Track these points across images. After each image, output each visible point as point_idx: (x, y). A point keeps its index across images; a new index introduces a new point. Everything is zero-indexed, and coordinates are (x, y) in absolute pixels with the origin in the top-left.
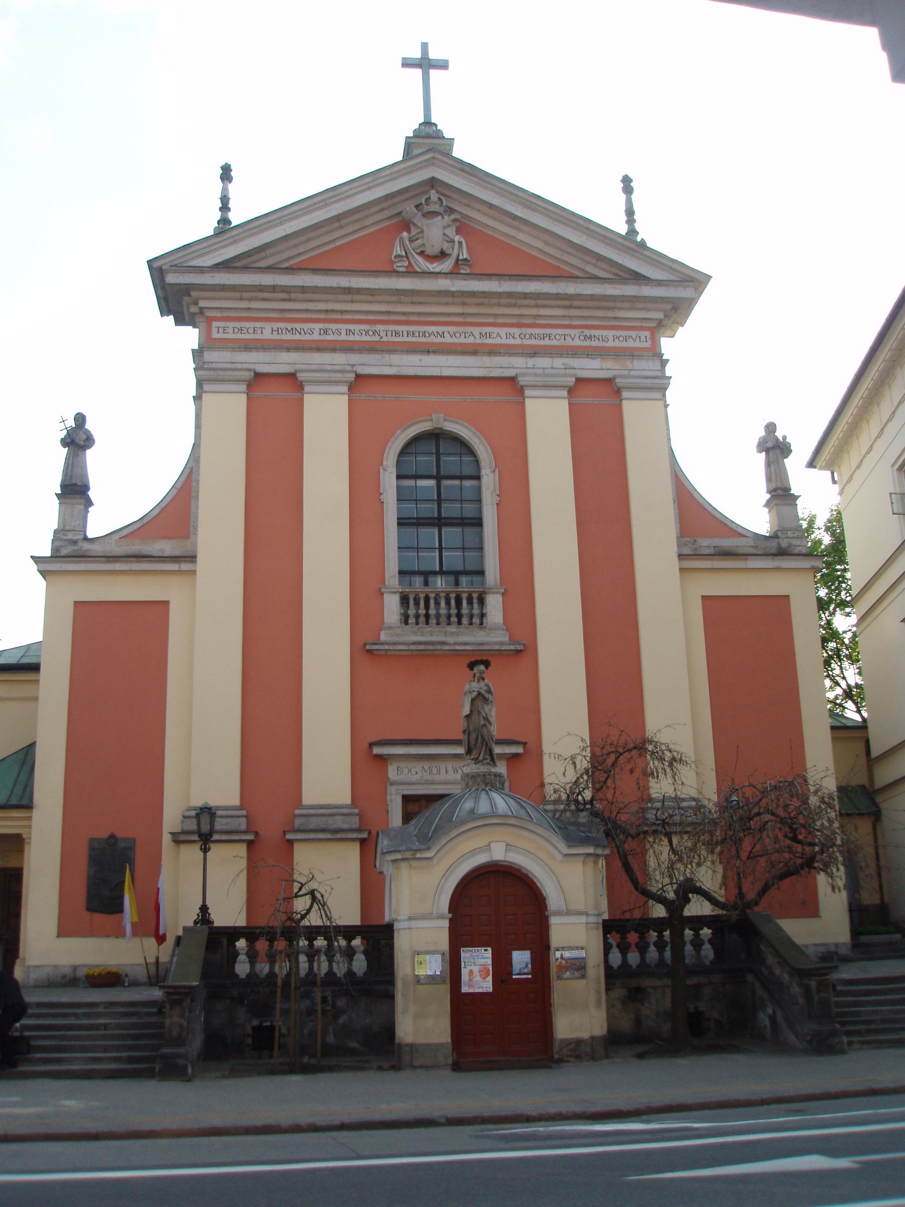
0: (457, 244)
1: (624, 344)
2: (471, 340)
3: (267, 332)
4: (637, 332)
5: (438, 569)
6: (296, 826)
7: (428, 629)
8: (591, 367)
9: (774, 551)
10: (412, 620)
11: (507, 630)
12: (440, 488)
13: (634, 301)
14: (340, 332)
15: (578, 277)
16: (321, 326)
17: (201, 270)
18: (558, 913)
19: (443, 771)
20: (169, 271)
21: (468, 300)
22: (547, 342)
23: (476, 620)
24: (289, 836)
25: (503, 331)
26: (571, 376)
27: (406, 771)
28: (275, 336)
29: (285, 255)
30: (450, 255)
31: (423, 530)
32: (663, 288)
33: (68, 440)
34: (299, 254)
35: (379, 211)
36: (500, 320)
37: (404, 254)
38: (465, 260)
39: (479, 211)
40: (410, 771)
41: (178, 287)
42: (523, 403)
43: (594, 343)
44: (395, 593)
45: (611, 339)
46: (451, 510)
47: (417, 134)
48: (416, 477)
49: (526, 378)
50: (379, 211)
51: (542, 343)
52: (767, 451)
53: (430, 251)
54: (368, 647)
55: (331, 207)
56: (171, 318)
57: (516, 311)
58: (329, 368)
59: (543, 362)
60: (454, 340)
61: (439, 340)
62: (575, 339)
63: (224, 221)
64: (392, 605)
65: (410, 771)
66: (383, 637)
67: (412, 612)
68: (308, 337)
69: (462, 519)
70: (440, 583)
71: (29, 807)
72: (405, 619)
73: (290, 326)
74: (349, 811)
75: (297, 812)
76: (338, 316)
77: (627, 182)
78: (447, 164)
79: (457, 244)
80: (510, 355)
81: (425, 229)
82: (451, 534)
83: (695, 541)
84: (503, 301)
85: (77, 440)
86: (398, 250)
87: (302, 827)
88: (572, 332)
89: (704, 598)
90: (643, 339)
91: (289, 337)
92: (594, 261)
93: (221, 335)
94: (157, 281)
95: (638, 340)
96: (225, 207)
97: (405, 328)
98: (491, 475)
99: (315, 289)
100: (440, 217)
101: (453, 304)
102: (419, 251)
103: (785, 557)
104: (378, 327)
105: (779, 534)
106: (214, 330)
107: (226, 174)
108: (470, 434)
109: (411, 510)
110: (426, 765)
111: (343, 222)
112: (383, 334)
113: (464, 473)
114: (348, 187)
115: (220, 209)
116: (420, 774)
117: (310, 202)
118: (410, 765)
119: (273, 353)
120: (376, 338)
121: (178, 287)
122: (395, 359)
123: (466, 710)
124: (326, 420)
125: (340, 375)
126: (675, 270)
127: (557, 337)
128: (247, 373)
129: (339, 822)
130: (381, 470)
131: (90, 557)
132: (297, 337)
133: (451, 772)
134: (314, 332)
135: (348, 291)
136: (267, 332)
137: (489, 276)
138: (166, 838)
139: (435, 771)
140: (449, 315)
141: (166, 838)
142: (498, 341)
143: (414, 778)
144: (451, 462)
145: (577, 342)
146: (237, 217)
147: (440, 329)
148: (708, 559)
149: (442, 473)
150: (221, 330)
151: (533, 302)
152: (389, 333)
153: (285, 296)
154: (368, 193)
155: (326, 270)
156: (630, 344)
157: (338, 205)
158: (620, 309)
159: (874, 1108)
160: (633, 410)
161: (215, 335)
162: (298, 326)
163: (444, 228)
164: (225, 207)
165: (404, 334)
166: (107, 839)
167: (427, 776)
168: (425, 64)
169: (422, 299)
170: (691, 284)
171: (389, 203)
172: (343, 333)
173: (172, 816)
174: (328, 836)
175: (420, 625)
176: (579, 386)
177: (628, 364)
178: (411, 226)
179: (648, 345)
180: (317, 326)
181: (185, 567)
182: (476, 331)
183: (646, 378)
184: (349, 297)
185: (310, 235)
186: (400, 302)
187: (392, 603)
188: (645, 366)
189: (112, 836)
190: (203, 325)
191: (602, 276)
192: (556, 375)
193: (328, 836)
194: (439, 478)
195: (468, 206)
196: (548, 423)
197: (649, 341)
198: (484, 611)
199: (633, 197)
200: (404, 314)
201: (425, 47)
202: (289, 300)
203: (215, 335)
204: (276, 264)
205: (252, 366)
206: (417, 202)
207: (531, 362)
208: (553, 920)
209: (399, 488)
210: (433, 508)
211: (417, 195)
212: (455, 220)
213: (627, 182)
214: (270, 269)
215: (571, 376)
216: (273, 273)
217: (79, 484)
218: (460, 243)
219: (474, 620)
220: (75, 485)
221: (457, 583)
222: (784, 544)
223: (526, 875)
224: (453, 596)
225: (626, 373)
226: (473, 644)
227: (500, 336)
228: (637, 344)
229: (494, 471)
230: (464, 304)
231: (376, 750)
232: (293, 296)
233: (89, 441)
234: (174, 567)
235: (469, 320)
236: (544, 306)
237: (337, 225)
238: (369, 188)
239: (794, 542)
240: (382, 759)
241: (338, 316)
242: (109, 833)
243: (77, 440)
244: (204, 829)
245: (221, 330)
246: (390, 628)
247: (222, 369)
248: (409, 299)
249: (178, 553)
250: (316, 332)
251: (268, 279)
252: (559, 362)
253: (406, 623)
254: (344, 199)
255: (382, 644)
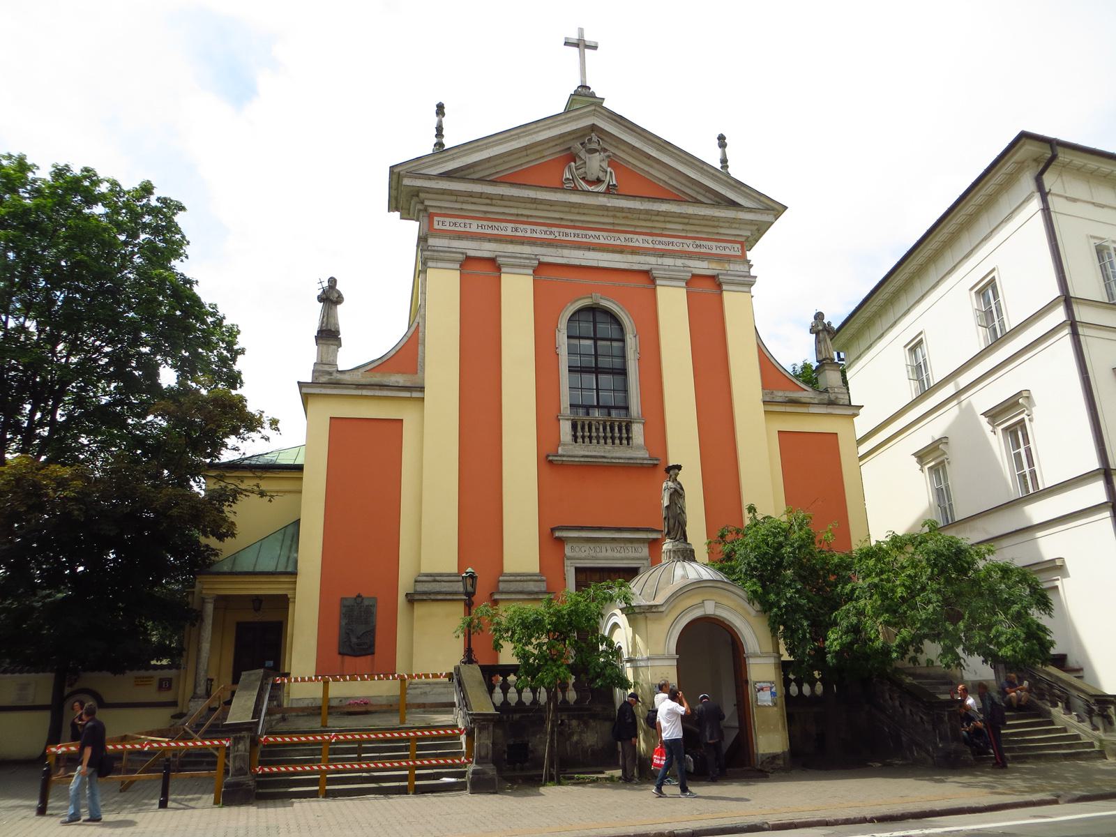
0: (609, 174)
1: (723, 252)
2: (618, 242)
3: (474, 227)
4: (732, 244)
5: (596, 404)
6: (501, 589)
7: (592, 447)
8: (702, 267)
9: (825, 402)
10: (580, 440)
11: (647, 450)
12: (598, 347)
13: (732, 222)
14: (526, 231)
15: (689, 202)
16: (513, 225)
17: (429, 177)
18: (755, 656)
19: (604, 550)
20: (406, 176)
21: (619, 214)
22: (670, 247)
23: (625, 442)
24: (496, 597)
25: (641, 238)
26: (688, 272)
27: (577, 549)
28: (480, 230)
29: (487, 173)
30: (604, 181)
31: (586, 376)
32: (753, 214)
33: (324, 296)
34: (497, 172)
35: (553, 146)
36: (638, 230)
37: (571, 178)
38: (614, 185)
39: (624, 151)
40: (580, 549)
41: (408, 191)
42: (655, 289)
43: (703, 250)
44: (567, 419)
45: (714, 248)
46: (604, 362)
47: (576, 93)
48: (580, 338)
49: (501, 259)
50: (553, 146)
51: (667, 247)
52: (817, 333)
53: (589, 177)
54: (550, 458)
55: (522, 140)
56: (397, 214)
57: (650, 224)
58: (519, 255)
59: (668, 261)
60: (606, 242)
61: (596, 241)
62: (690, 246)
63: (440, 145)
64: (566, 428)
65: (580, 549)
66: (560, 451)
67: (579, 434)
68: (503, 233)
69: (613, 369)
70: (596, 414)
71: (296, 574)
72: (575, 438)
73: (490, 224)
74: (539, 578)
75: (501, 578)
76: (525, 219)
77: (722, 139)
78: (602, 113)
79: (609, 174)
80: (646, 255)
81: (587, 161)
82: (606, 380)
83: (772, 392)
84: (642, 216)
85: (330, 297)
86: (568, 175)
87: (505, 590)
88: (688, 241)
89: (779, 432)
90: (736, 249)
91: (489, 231)
92: (704, 193)
93: (440, 227)
94: (394, 184)
95: (732, 250)
96: (439, 131)
97: (572, 231)
98: (633, 339)
99: (512, 198)
100: (598, 153)
101: (607, 216)
102: (581, 177)
103: (835, 406)
104: (553, 229)
105: (829, 389)
106: (436, 223)
107: (440, 109)
108: (618, 309)
109: (577, 361)
110: (592, 546)
111: (529, 152)
112: (557, 234)
113: (614, 337)
114: (534, 126)
115: (436, 136)
116: (587, 552)
117: (508, 134)
118: (614, 545)
119: (479, 243)
120: (552, 237)
121: (408, 191)
122: (566, 252)
123: (666, 502)
124: (517, 292)
125: (528, 261)
126: (761, 202)
127: (677, 245)
128: (461, 256)
129: (532, 586)
130: (557, 331)
131: (341, 384)
132: (496, 232)
133: (609, 551)
134: (508, 230)
135: (534, 201)
136: (474, 227)
137: (634, 197)
138: (401, 598)
139: (598, 550)
140: (603, 223)
141: (401, 598)
142: (637, 244)
143: (583, 555)
144: (605, 328)
145: (691, 249)
146: (449, 142)
147: (597, 233)
148: (783, 405)
149: (598, 336)
150: (440, 223)
151: (662, 219)
152: (561, 234)
153: (488, 201)
154: (548, 131)
155: (520, 184)
156: (727, 252)
157: (527, 138)
158: (721, 227)
159: (379, 753)
160: (731, 299)
161: (436, 226)
162: (496, 224)
163: (601, 161)
164: (439, 131)
165: (572, 235)
166: (355, 599)
167: (592, 553)
168: (580, 44)
169: (586, 211)
170: (772, 212)
171: (561, 141)
172: (529, 231)
173: (405, 582)
174: (525, 597)
175: (586, 444)
176: (694, 280)
177: (726, 265)
178: (577, 159)
179: (739, 253)
180: (510, 225)
181: (415, 395)
182: (622, 236)
183: (740, 276)
184: (534, 206)
185: (506, 159)
186: (570, 212)
187: (566, 427)
188: (739, 268)
189: (359, 596)
190: (426, 220)
191: (706, 202)
192: (679, 271)
193: (525, 597)
194: (595, 339)
195: (616, 147)
196: (672, 304)
197: (740, 251)
198: (630, 435)
199: (726, 149)
200: (572, 221)
201: (581, 31)
202: (491, 205)
203: (436, 226)
204: (483, 177)
205: (464, 251)
206: (582, 142)
207: (660, 261)
208: (751, 661)
209: (569, 345)
210: (591, 361)
211: (581, 136)
212: (609, 156)
213: (722, 139)
214: (481, 180)
215: (688, 272)
216: (480, 183)
217: (333, 330)
218: (611, 173)
219: (623, 441)
220: (330, 330)
221: (609, 414)
222: (832, 397)
223: (728, 625)
224: (608, 423)
225: (725, 272)
226: (625, 459)
227: (639, 241)
228: (732, 253)
229: (635, 336)
230: (614, 217)
231: (558, 534)
232: (494, 202)
233: (339, 299)
234: (407, 394)
235: (616, 228)
236: (669, 222)
237: (524, 153)
238: (549, 128)
239: (840, 396)
240: (561, 541)
241: (525, 219)
242: (357, 594)
243: (330, 297)
244: (427, 593)
245: (440, 223)
246: (564, 445)
247: (442, 251)
248: (576, 211)
249: (408, 384)
250: (509, 230)
251: (478, 188)
252: (679, 262)
253: (576, 442)
254: (531, 134)
255: (561, 456)
